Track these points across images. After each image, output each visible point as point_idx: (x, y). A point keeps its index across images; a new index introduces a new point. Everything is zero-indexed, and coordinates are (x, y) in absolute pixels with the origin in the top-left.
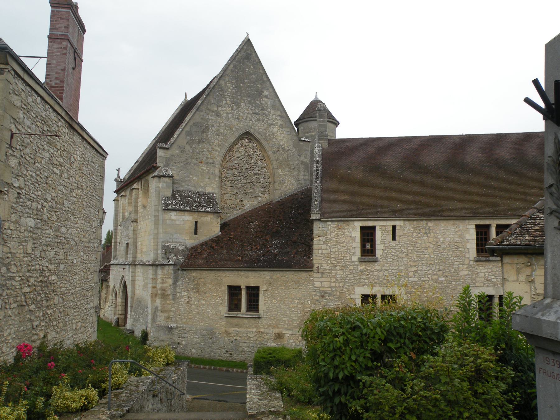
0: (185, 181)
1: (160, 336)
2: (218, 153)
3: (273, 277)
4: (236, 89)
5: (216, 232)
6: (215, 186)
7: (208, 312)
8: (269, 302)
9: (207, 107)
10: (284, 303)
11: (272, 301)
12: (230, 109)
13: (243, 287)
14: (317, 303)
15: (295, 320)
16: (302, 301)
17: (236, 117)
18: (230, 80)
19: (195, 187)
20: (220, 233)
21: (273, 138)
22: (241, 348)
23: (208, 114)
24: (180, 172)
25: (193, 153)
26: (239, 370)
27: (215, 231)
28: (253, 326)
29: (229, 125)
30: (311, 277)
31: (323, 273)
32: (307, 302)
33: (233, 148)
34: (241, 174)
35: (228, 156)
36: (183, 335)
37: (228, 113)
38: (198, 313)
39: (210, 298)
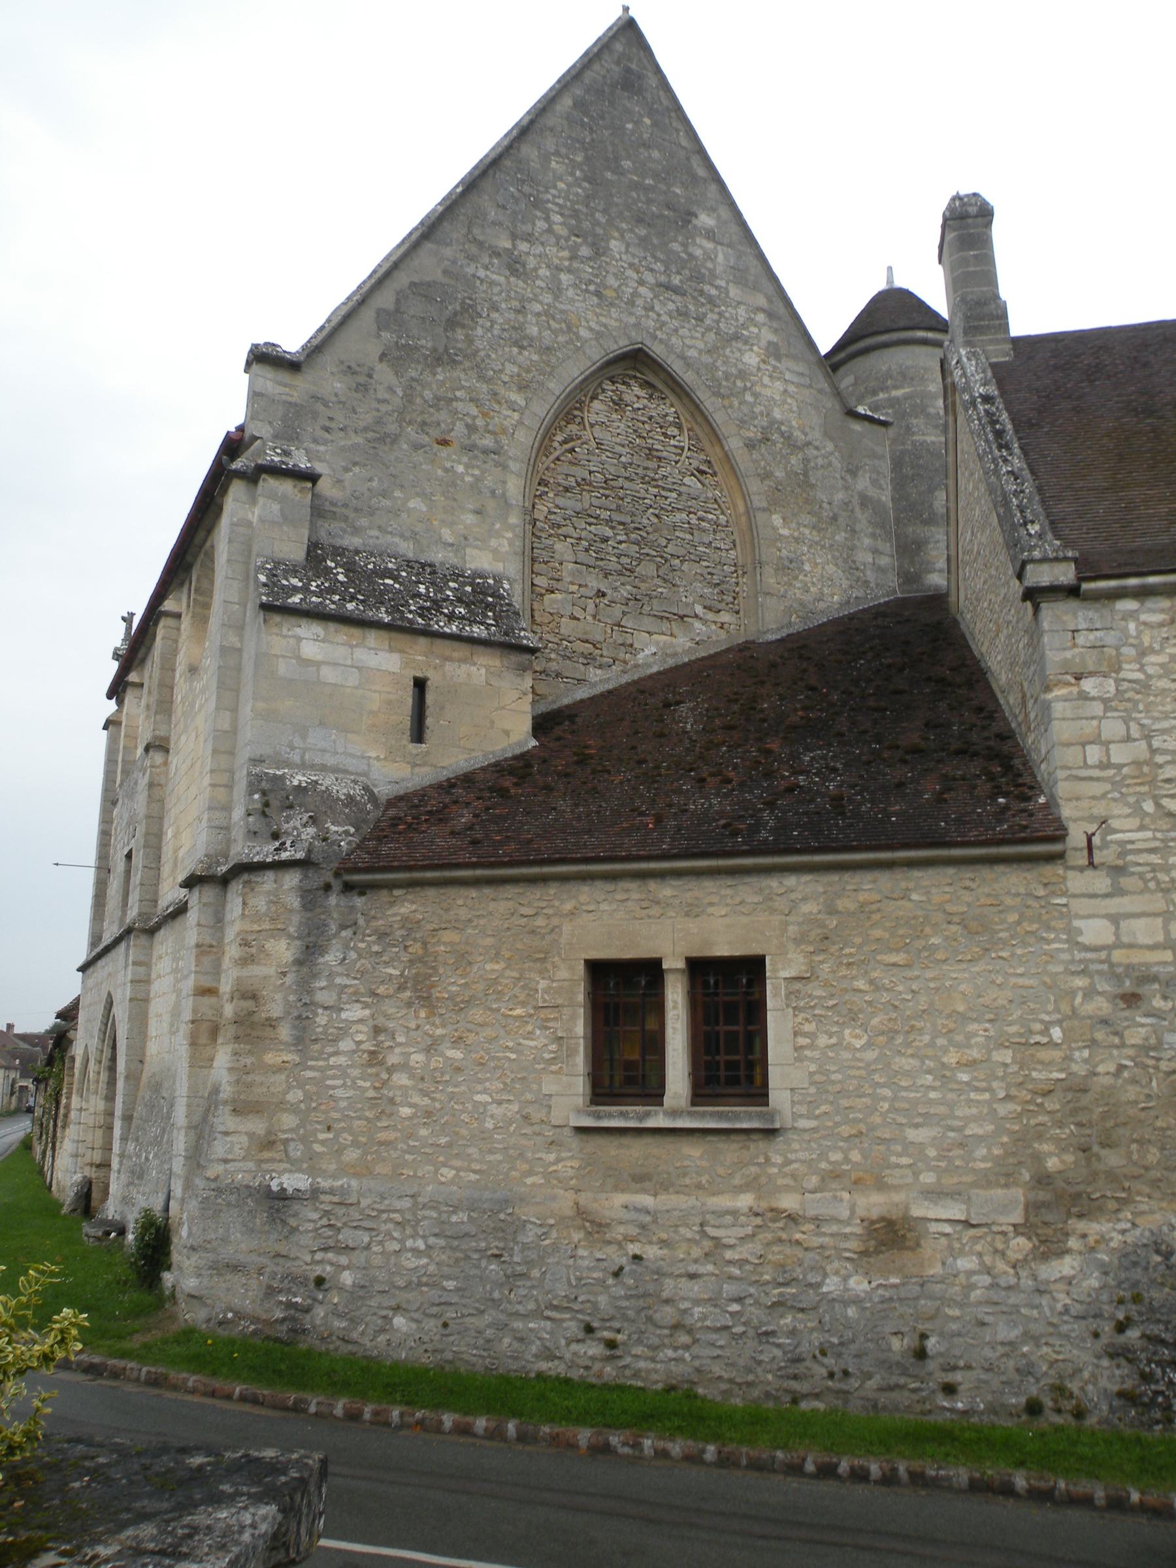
0: (372, 513)
1: (225, 1240)
2: (516, 416)
3: (841, 904)
4: (586, 185)
5: (514, 738)
6: (505, 547)
7: (480, 1111)
8: (823, 1040)
9: (469, 231)
10: (908, 1045)
11: (840, 1035)
12: (566, 254)
13: (673, 963)
14: (1099, 1035)
15: (980, 1139)
16: (1013, 1029)
17: (592, 288)
18: (563, 151)
19: (416, 541)
20: (533, 743)
21: (745, 389)
22: (668, 1309)
23: (471, 258)
24: (347, 470)
25: (409, 398)
26: (676, 1448)
27: (507, 733)
28: (737, 1181)
29: (562, 312)
30: (1054, 894)
31: (1118, 871)
32: (1046, 1032)
33: (581, 409)
34: (617, 517)
35: (559, 438)
36: (347, 1236)
37: (559, 269)
38: (429, 1114)
39: (488, 1032)
